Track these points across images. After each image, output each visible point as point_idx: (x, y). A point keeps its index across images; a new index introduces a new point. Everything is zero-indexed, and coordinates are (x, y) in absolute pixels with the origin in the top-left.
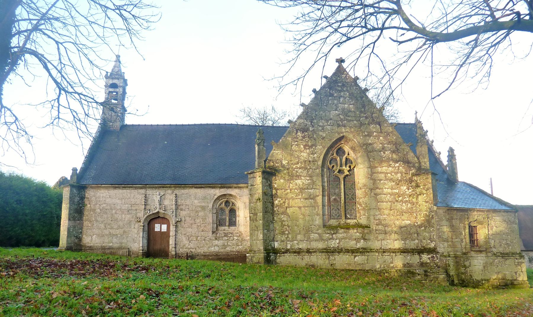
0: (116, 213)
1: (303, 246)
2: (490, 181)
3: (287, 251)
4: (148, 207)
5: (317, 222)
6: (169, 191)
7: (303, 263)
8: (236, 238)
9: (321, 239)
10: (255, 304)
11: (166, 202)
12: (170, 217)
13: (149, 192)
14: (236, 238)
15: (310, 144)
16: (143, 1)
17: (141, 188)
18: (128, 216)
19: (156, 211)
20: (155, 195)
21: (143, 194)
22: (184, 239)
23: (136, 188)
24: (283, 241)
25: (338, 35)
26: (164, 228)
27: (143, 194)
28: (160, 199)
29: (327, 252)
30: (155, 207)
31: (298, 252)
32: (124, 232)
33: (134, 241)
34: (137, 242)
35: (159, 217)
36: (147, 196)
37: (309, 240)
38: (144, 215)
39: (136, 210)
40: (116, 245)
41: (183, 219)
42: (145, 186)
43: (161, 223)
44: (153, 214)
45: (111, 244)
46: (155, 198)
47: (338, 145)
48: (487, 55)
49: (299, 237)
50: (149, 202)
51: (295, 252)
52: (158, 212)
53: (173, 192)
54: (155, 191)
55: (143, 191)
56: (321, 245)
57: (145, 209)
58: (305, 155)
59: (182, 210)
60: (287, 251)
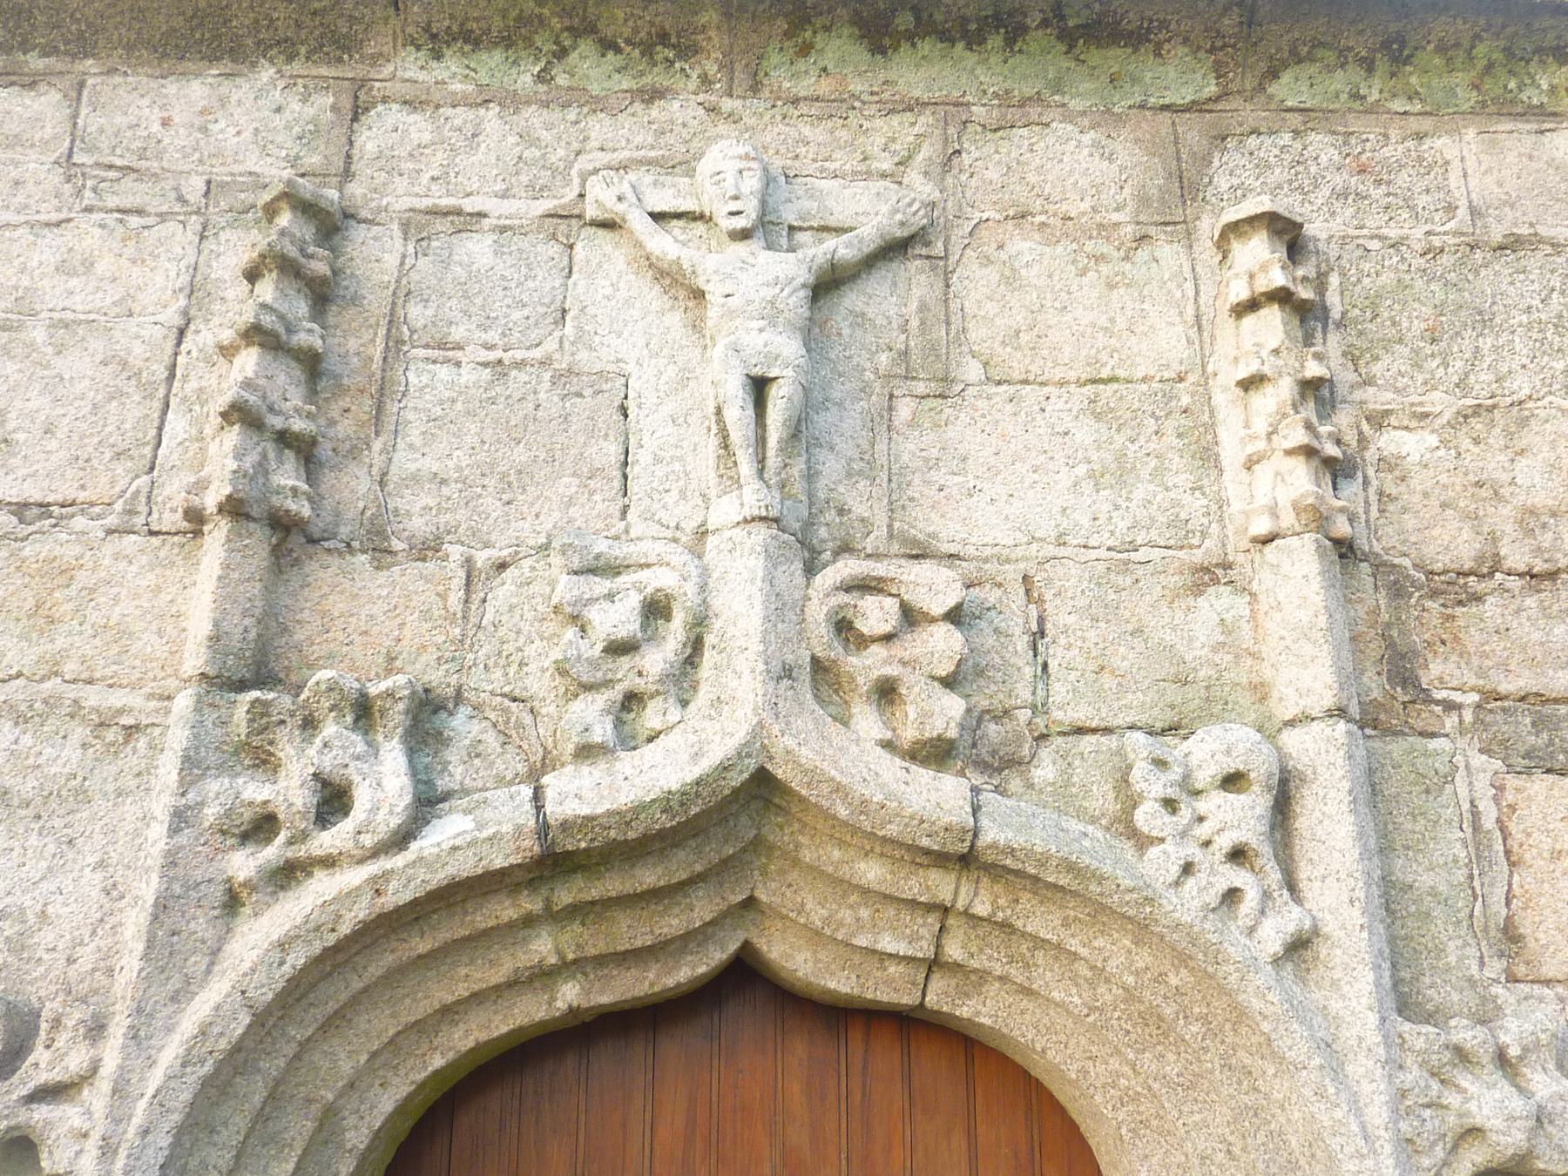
2: (1304, 872)
4: (370, 622)
10: (1156, 1086)
11: (1000, 485)
12: (1186, 996)
13: (452, 146)
19: (669, 763)
21: (213, 203)
25: (954, 951)
27: (213, 203)
35: (745, 976)
36: (376, 255)
38: (195, 911)
44: (556, 860)
50: (430, 448)
52: (753, 799)
53: (1187, 187)
54: (626, 131)
55: (247, 122)
57: (253, 667)
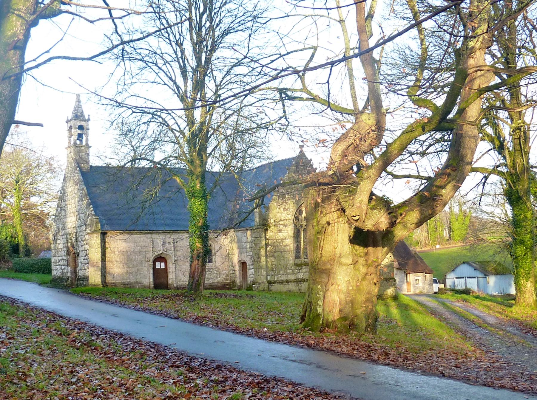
0: (131, 255)
1: (284, 278)
3: (275, 282)
5: (291, 262)
6: (168, 236)
7: (284, 290)
8: (216, 272)
9: (293, 273)
13: (154, 236)
14: (216, 272)
15: (286, 208)
16: (74, 1)
17: (148, 233)
18: (140, 257)
20: (159, 239)
22: (180, 274)
23: (145, 234)
24: (272, 275)
26: (163, 265)
28: (160, 242)
29: (297, 282)
30: (160, 250)
31: (281, 282)
32: (138, 270)
33: (145, 277)
34: (148, 279)
37: (287, 274)
39: (146, 251)
40: (132, 281)
41: (179, 258)
42: (151, 232)
43: (160, 262)
45: (128, 281)
46: (159, 242)
47: (445, 250)
48: (166, 26)
49: (281, 272)
51: (280, 283)
55: (149, 236)
56: (292, 277)
58: (284, 215)
59: (177, 251)
60: (275, 282)
